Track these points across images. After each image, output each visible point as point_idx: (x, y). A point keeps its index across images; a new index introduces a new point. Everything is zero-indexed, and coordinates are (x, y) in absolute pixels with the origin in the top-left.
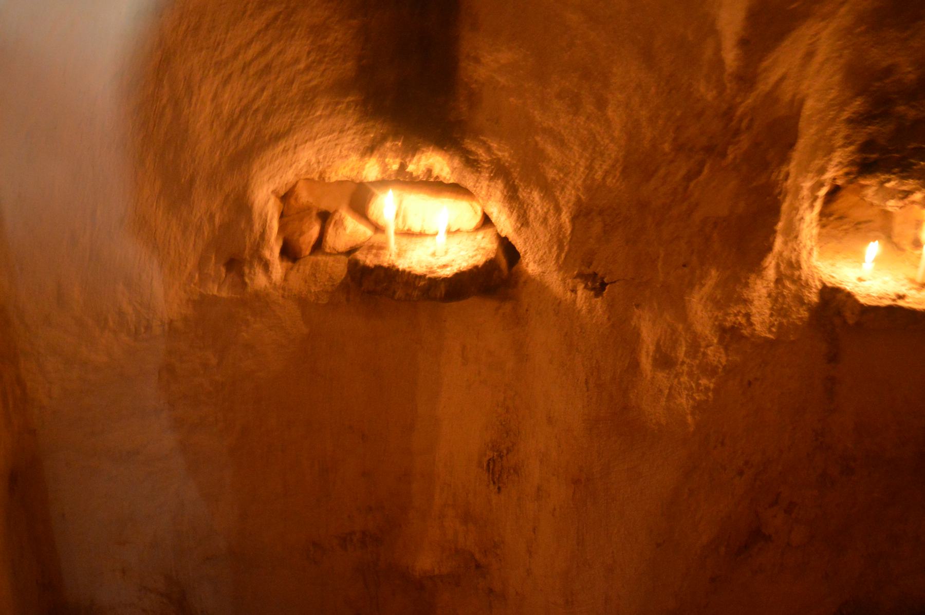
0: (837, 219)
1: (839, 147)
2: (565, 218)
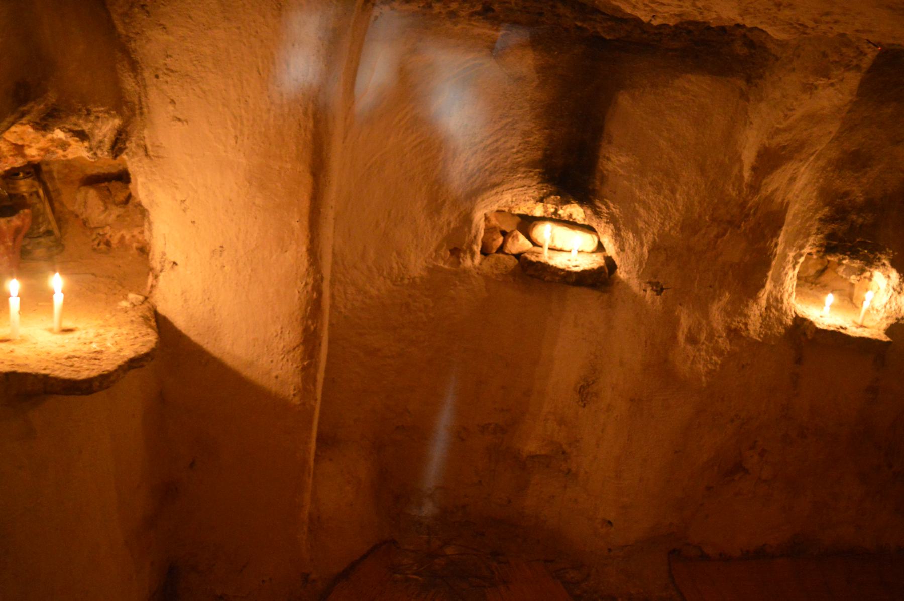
0: (813, 282)
2: (645, 249)
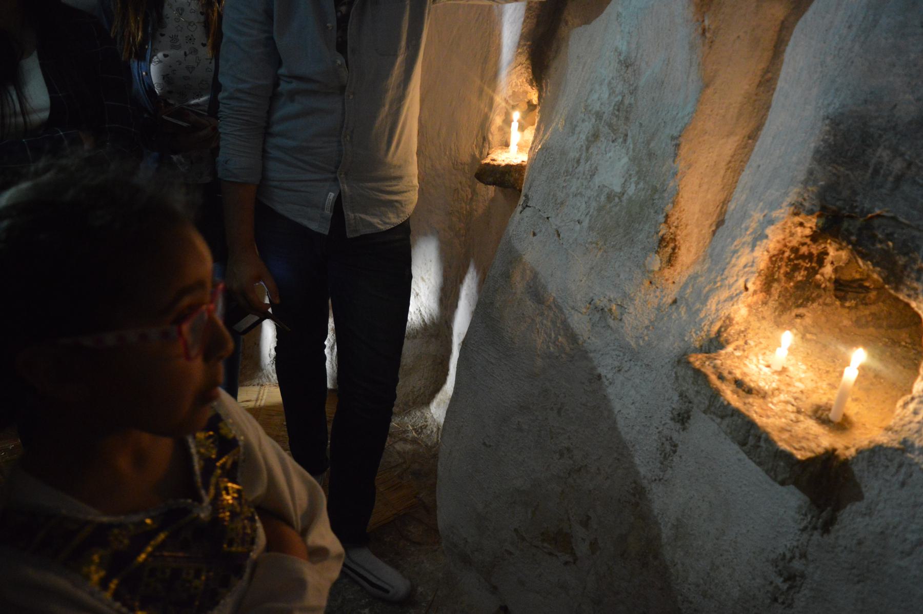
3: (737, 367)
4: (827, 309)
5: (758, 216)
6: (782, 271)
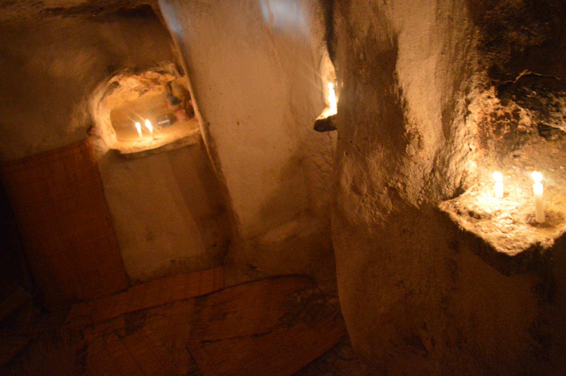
1: (477, 71)
3: (470, 203)
4: (537, 146)
5: (462, 101)
6: (491, 131)
